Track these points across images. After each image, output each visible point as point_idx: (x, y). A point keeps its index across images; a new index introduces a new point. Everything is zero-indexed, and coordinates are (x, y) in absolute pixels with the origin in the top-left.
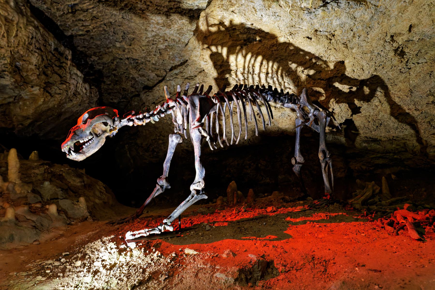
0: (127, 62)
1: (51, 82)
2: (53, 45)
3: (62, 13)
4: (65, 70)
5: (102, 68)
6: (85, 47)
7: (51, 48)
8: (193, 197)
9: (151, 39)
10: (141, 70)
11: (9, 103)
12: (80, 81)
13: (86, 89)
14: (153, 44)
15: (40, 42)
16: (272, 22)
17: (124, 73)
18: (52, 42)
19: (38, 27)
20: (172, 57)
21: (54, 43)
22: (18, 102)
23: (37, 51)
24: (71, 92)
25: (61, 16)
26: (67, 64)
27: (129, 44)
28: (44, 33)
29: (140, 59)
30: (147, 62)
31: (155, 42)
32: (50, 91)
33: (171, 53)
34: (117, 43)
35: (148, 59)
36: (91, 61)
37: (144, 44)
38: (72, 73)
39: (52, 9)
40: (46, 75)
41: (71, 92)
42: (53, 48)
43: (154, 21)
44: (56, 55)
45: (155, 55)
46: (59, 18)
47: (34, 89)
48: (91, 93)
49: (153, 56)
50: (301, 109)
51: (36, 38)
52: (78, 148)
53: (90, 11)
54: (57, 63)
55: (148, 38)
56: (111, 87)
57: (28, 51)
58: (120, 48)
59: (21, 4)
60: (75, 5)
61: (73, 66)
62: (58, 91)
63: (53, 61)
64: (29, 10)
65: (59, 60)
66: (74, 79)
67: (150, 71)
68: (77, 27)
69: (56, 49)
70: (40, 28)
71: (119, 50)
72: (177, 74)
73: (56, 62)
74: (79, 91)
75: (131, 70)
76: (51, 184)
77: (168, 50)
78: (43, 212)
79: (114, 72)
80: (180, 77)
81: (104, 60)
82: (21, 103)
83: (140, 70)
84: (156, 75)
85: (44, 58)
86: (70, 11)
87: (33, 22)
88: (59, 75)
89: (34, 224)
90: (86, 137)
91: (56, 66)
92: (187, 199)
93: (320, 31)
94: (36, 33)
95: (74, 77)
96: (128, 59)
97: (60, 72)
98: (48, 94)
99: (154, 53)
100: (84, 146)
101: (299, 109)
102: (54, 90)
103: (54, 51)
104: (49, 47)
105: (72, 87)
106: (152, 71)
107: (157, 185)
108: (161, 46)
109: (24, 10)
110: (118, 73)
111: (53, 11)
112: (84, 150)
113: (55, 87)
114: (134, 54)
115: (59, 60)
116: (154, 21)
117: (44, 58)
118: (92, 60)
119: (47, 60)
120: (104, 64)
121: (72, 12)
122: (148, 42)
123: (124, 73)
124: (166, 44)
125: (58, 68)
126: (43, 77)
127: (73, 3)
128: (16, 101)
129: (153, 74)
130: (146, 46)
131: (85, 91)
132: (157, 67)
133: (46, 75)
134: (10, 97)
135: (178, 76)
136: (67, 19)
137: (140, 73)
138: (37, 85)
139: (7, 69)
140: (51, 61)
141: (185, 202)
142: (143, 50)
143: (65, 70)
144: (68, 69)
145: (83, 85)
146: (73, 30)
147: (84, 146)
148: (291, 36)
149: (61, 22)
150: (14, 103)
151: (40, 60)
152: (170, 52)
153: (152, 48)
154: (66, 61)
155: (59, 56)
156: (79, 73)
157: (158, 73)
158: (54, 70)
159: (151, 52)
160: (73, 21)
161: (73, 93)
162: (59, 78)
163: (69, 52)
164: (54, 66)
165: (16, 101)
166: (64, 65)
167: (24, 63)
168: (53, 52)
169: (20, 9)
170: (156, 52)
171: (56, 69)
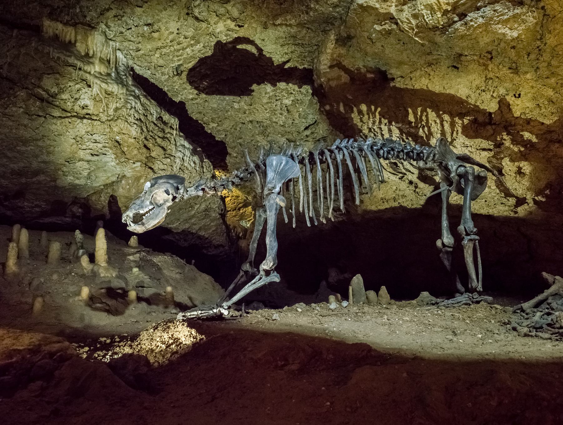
0: (250, 126)
1: (153, 156)
2: (155, 114)
3: (167, 76)
4: (169, 141)
5: (223, 136)
6: (200, 113)
7: (153, 117)
8: (261, 278)
9: (271, 94)
10: (270, 135)
11: (113, 182)
12: (188, 153)
13: (194, 163)
14: (277, 100)
15: (140, 112)
16: (397, 53)
17: (252, 140)
18: (154, 110)
19: (138, 96)
20: (303, 114)
21: (157, 112)
22: (121, 181)
23: (136, 122)
24: (176, 167)
25: (166, 80)
26: (173, 135)
27: (250, 104)
28: (145, 101)
29: (264, 121)
30: (274, 124)
31: (278, 98)
32: (153, 167)
33: (301, 109)
34: (235, 104)
35: (274, 120)
36: (210, 129)
37: (265, 101)
38: (178, 144)
39: (157, 74)
40: (148, 149)
41: (176, 167)
42: (155, 117)
43: (270, 72)
44: (159, 125)
45: (281, 114)
46: (165, 83)
47: (135, 165)
48: (203, 167)
49: (279, 115)
50: (443, 168)
51: (135, 108)
52: (138, 219)
53: (198, 69)
54: (161, 135)
55: (269, 93)
56: (237, 160)
57: (126, 123)
58: (240, 109)
59: (123, 74)
60: (179, 65)
61: (180, 136)
62: (162, 167)
63: (155, 132)
64: (130, 78)
65: (163, 131)
66: (180, 151)
67: (279, 135)
68: (186, 91)
69: (160, 118)
70: (141, 96)
71: (239, 112)
72: (307, 136)
73: (159, 133)
74: (186, 165)
75: (257, 136)
76: (139, 270)
77: (297, 105)
78: (123, 299)
79: (240, 141)
80: (311, 140)
81: (225, 126)
82: (123, 182)
83: (268, 136)
84: (287, 139)
85: (145, 130)
86: (175, 73)
87: (134, 91)
88: (162, 148)
89: (107, 308)
90: (146, 207)
91: (159, 137)
92: (253, 281)
93: (466, 56)
94: (136, 103)
95: (180, 149)
96: (251, 122)
97: (164, 144)
98: (149, 170)
99: (280, 111)
100: (144, 217)
101: (440, 168)
102: (157, 165)
103: (156, 120)
104: (151, 116)
105: (178, 161)
106: (283, 136)
107: (241, 271)
108: (288, 102)
109: (125, 80)
110: (244, 142)
111: (158, 75)
112: (144, 221)
113: (159, 162)
114: (256, 115)
115: (163, 131)
116: (270, 72)
117: (145, 130)
118: (211, 127)
119: (148, 131)
120: (224, 130)
121: (178, 74)
122: (269, 98)
123: (252, 140)
124: (292, 98)
125: (161, 140)
126: (145, 150)
127: (177, 64)
128: (119, 180)
129: (284, 139)
130: (267, 103)
131: (193, 165)
132: (288, 130)
133: (148, 149)
134: (112, 176)
135: (308, 139)
136: (174, 83)
137: (269, 139)
138: (138, 161)
139: (107, 145)
140: (153, 133)
141: (250, 284)
142: (266, 110)
143: (169, 141)
144: (173, 140)
145: (191, 157)
146: (182, 95)
147: (144, 217)
148: (430, 68)
149: (167, 87)
150: (117, 182)
151: (139, 131)
152: (299, 108)
153: (276, 105)
154: (171, 131)
155: (162, 126)
156: (187, 144)
157: (290, 137)
158: (156, 142)
159: (276, 111)
160: (180, 84)
161: (180, 168)
162: (162, 152)
163: (175, 121)
164: (156, 137)
165: (119, 180)
166: (169, 135)
167: (124, 136)
168: (156, 122)
169: (121, 78)
170: (281, 109)
171: (159, 140)
